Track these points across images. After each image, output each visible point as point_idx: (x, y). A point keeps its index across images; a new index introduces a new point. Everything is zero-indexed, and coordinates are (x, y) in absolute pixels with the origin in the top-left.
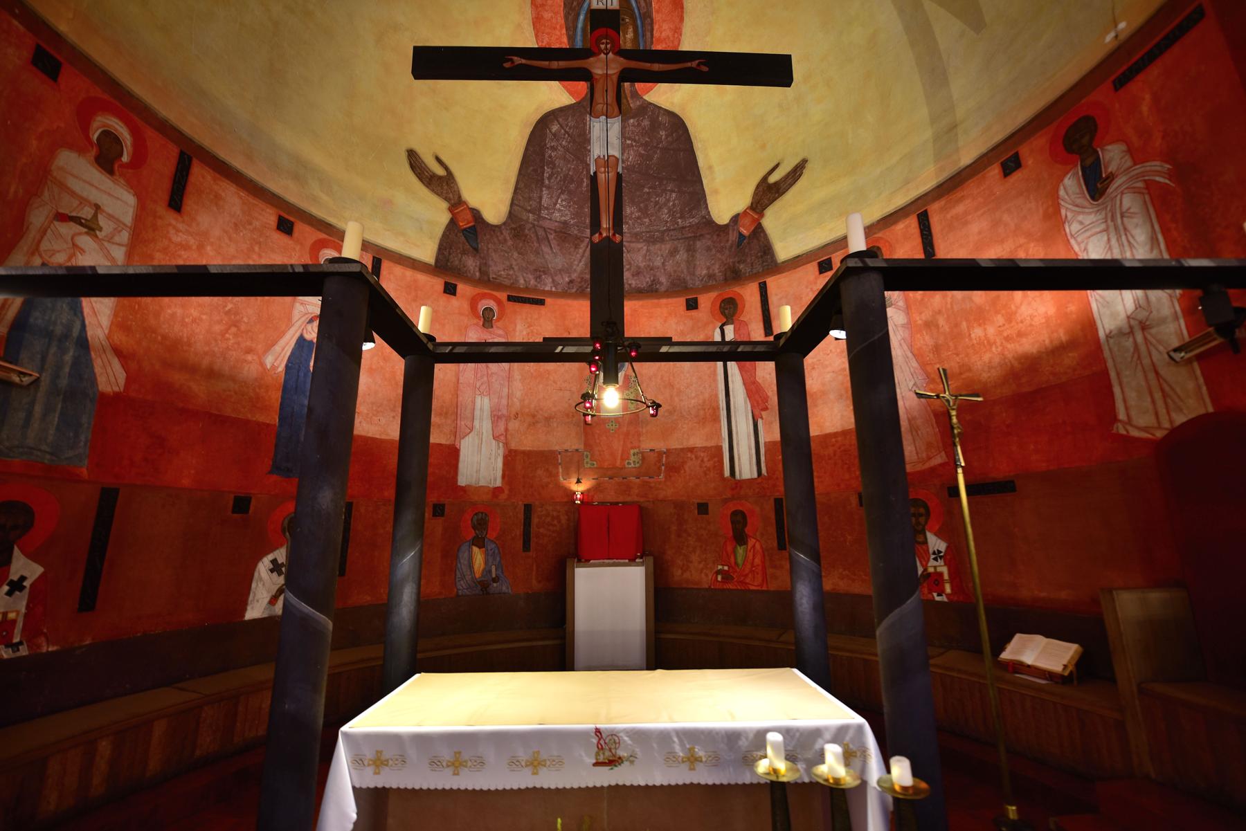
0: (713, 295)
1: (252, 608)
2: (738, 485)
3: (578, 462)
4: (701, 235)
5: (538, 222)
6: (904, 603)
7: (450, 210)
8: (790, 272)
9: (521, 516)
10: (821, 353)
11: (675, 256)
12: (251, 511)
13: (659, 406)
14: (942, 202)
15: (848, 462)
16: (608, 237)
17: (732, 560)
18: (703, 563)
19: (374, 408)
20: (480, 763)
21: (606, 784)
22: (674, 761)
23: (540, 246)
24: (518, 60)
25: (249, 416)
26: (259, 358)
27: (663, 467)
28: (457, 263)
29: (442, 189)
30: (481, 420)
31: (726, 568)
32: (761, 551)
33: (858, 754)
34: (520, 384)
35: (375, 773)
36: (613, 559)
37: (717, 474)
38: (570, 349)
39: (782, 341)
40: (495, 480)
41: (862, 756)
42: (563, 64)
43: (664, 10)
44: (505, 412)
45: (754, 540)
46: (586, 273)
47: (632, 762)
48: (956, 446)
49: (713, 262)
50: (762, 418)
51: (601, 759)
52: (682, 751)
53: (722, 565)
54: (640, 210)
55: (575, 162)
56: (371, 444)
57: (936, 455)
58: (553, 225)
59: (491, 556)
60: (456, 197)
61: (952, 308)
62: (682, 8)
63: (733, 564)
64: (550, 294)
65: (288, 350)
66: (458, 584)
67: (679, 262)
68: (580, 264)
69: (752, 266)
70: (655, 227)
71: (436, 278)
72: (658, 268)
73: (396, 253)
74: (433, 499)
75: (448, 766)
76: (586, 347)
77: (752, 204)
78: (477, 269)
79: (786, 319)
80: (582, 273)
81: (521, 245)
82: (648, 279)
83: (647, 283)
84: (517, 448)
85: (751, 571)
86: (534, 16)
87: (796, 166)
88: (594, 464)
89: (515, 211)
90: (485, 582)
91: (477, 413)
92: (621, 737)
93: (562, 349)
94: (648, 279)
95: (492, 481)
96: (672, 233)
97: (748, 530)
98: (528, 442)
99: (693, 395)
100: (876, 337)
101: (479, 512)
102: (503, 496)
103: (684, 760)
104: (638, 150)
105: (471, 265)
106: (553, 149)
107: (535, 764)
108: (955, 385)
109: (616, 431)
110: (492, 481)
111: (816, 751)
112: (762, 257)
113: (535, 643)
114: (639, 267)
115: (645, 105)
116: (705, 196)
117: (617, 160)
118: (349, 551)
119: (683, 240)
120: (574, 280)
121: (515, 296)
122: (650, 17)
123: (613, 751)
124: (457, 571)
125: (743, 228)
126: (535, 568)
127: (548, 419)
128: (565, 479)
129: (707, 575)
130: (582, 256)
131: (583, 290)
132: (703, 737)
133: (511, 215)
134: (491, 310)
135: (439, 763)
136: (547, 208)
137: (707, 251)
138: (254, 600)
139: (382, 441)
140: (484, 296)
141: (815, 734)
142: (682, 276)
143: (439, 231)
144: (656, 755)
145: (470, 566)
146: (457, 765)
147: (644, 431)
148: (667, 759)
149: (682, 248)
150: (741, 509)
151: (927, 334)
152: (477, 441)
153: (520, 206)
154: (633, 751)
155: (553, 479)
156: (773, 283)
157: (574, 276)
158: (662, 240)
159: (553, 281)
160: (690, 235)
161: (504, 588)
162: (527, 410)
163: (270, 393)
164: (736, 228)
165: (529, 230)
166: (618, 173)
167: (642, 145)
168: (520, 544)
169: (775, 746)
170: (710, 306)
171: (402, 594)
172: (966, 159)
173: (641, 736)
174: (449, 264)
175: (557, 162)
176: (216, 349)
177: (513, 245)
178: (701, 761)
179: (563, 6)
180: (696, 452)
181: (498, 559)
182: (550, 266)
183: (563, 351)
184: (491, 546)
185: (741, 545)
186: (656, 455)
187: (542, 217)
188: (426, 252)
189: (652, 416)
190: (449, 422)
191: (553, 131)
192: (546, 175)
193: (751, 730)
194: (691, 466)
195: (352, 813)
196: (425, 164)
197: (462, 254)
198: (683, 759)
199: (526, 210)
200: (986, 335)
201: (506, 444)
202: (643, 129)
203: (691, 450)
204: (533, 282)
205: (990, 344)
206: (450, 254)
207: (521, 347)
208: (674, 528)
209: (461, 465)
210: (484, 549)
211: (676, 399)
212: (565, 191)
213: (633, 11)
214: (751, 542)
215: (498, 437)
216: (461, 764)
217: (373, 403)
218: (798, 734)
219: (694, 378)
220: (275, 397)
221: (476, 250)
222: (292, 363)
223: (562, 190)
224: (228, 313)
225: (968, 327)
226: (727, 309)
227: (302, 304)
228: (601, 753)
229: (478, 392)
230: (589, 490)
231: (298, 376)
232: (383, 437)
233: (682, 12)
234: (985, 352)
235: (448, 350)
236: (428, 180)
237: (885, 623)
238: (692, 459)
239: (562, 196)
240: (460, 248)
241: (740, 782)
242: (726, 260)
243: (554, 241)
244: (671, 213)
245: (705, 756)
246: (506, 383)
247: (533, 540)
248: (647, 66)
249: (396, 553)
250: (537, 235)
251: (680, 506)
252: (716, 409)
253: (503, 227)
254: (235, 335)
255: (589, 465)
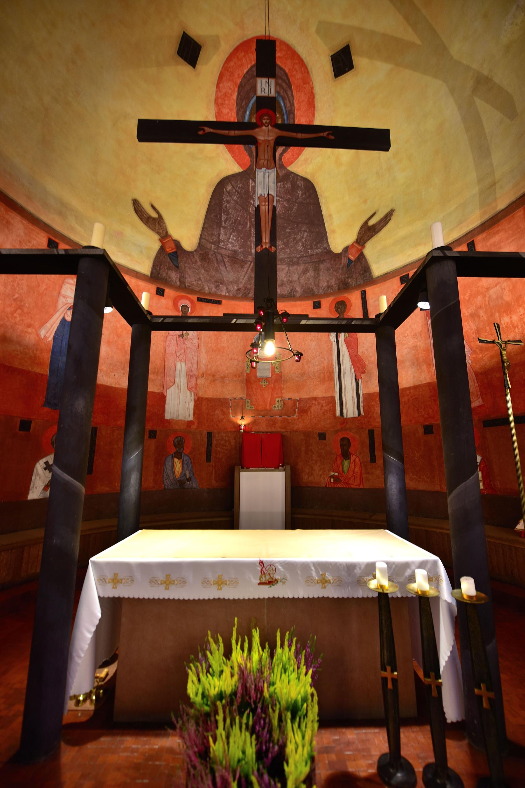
0: (331, 299)
1: (33, 492)
2: (344, 421)
3: (242, 405)
4: (323, 260)
5: (218, 250)
6: (468, 478)
7: (161, 240)
8: (382, 283)
9: (205, 440)
10: (401, 336)
11: (306, 274)
12: (31, 430)
13: (302, 354)
14: (484, 235)
15: (417, 406)
16: (266, 248)
17: (341, 469)
18: (322, 471)
19: (111, 367)
20: (183, 582)
21: (266, 597)
22: (312, 583)
23: (218, 266)
24: (208, 130)
25: (30, 368)
26: (36, 331)
27: (297, 410)
28: (165, 275)
29: (155, 226)
30: (180, 377)
31: (336, 474)
32: (359, 463)
33: (434, 579)
34: (205, 355)
35: (113, 588)
36: (264, 467)
37: (331, 414)
38: (241, 321)
39: (381, 317)
40: (189, 416)
41: (436, 581)
42: (237, 133)
43: (302, 109)
44: (195, 372)
45: (355, 457)
46: (248, 284)
47: (284, 583)
48: (506, 375)
49: (331, 277)
50: (361, 378)
51: (263, 580)
52: (317, 576)
53: (334, 472)
54: (284, 243)
55: (242, 211)
56: (109, 391)
57: (476, 400)
58: (227, 253)
59: (186, 464)
60: (164, 232)
61: (489, 304)
62: (314, 107)
63: (341, 471)
64: (225, 297)
65: (55, 327)
66: (165, 482)
67: (309, 277)
68: (245, 279)
69: (356, 280)
70: (294, 255)
71: (151, 284)
72: (295, 282)
73: (125, 267)
74: (149, 427)
75: (162, 584)
76: (252, 320)
77: (357, 239)
78: (178, 280)
79: (384, 305)
80: (245, 284)
81: (206, 265)
82: (288, 289)
83: (288, 291)
84: (203, 396)
85: (353, 476)
86: (216, 111)
87: (388, 213)
88: (252, 408)
89: (202, 242)
90: (182, 481)
91: (178, 373)
92: (277, 566)
93: (236, 321)
94: (288, 289)
95: (187, 416)
96: (304, 259)
97: (351, 450)
98: (210, 393)
99: (317, 363)
100: (452, 303)
101: (179, 436)
102: (194, 427)
103: (318, 582)
104: (283, 204)
105: (174, 277)
106: (228, 202)
107: (220, 583)
108: (490, 355)
109: (266, 387)
110: (187, 416)
111: (406, 577)
112: (363, 274)
113: (214, 519)
114: (282, 281)
115: (288, 174)
116: (327, 235)
117: (273, 197)
118: (95, 458)
119: (312, 264)
120: (240, 288)
121: (202, 298)
122: (293, 113)
123: (272, 575)
124: (164, 474)
125: (351, 255)
126: (214, 472)
127: (223, 378)
128: (234, 417)
129: (324, 478)
130: (246, 273)
131: (246, 295)
132: (331, 567)
133: (200, 245)
134: (186, 306)
135: (156, 582)
136: (223, 242)
137: (327, 271)
138: (34, 487)
139: (116, 389)
140: (182, 297)
141: (406, 565)
142: (311, 286)
143: (153, 254)
144: (300, 578)
145: (173, 471)
146: (168, 583)
147: (285, 386)
148: (307, 581)
149: (311, 268)
150: (346, 436)
151: (472, 322)
152: (177, 391)
153: (205, 239)
154: (285, 575)
155: (226, 416)
156: (369, 290)
157: (241, 286)
158: (298, 263)
159: (227, 289)
160: (316, 260)
161: (194, 485)
162: (209, 372)
163: (43, 354)
164: (346, 255)
165: (212, 255)
166: (274, 206)
167: (286, 200)
168: (204, 457)
169: (381, 570)
170: (329, 306)
171: (130, 479)
172: (501, 205)
173: (290, 566)
174: (159, 276)
175: (230, 211)
176: (8, 323)
177: (201, 265)
178: (330, 583)
179: (235, 104)
180: (319, 400)
181: (191, 466)
182: (225, 279)
183: (236, 320)
184: (186, 458)
185: (346, 460)
186: (292, 402)
187: (220, 247)
188: (145, 268)
189: (297, 361)
190: (159, 378)
191: (228, 190)
192: (223, 219)
193: (363, 563)
194: (315, 409)
195: (98, 613)
196: (144, 209)
197: (168, 270)
198: (317, 581)
199: (210, 242)
200: (511, 321)
201: (196, 393)
202: (287, 189)
203: (315, 399)
204: (214, 289)
205: (514, 327)
206: (160, 269)
207: (209, 319)
208: (303, 449)
209: (167, 406)
210: (181, 460)
211: (306, 366)
212: (235, 230)
213: (282, 109)
214: (353, 458)
215: (191, 389)
216: (170, 583)
217: (110, 364)
218: (394, 566)
219: (318, 353)
220: (47, 357)
221: (177, 267)
222: (57, 336)
223: (233, 230)
224: (16, 300)
225: (500, 317)
226: (339, 308)
227: (64, 297)
228: (263, 576)
229: (178, 360)
230: (249, 424)
231: (62, 344)
232: (117, 386)
233: (314, 110)
234: (510, 333)
235: (160, 320)
236: (146, 220)
237: (454, 493)
238: (315, 405)
239: (233, 234)
240: (167, 265)
241: (355, 596)
242: (340, 276)
243: (228, 263)
244: (304, 246)
245: (332, 580)
246: (196, 354)
247: (213, 455)
248: (293, 135)
249: (125, 452)
250: (217, 259)
251: (307, 435)
252: (331, 373)
253: (195, 253)
254: (21, 315)
255: (249, 408)
